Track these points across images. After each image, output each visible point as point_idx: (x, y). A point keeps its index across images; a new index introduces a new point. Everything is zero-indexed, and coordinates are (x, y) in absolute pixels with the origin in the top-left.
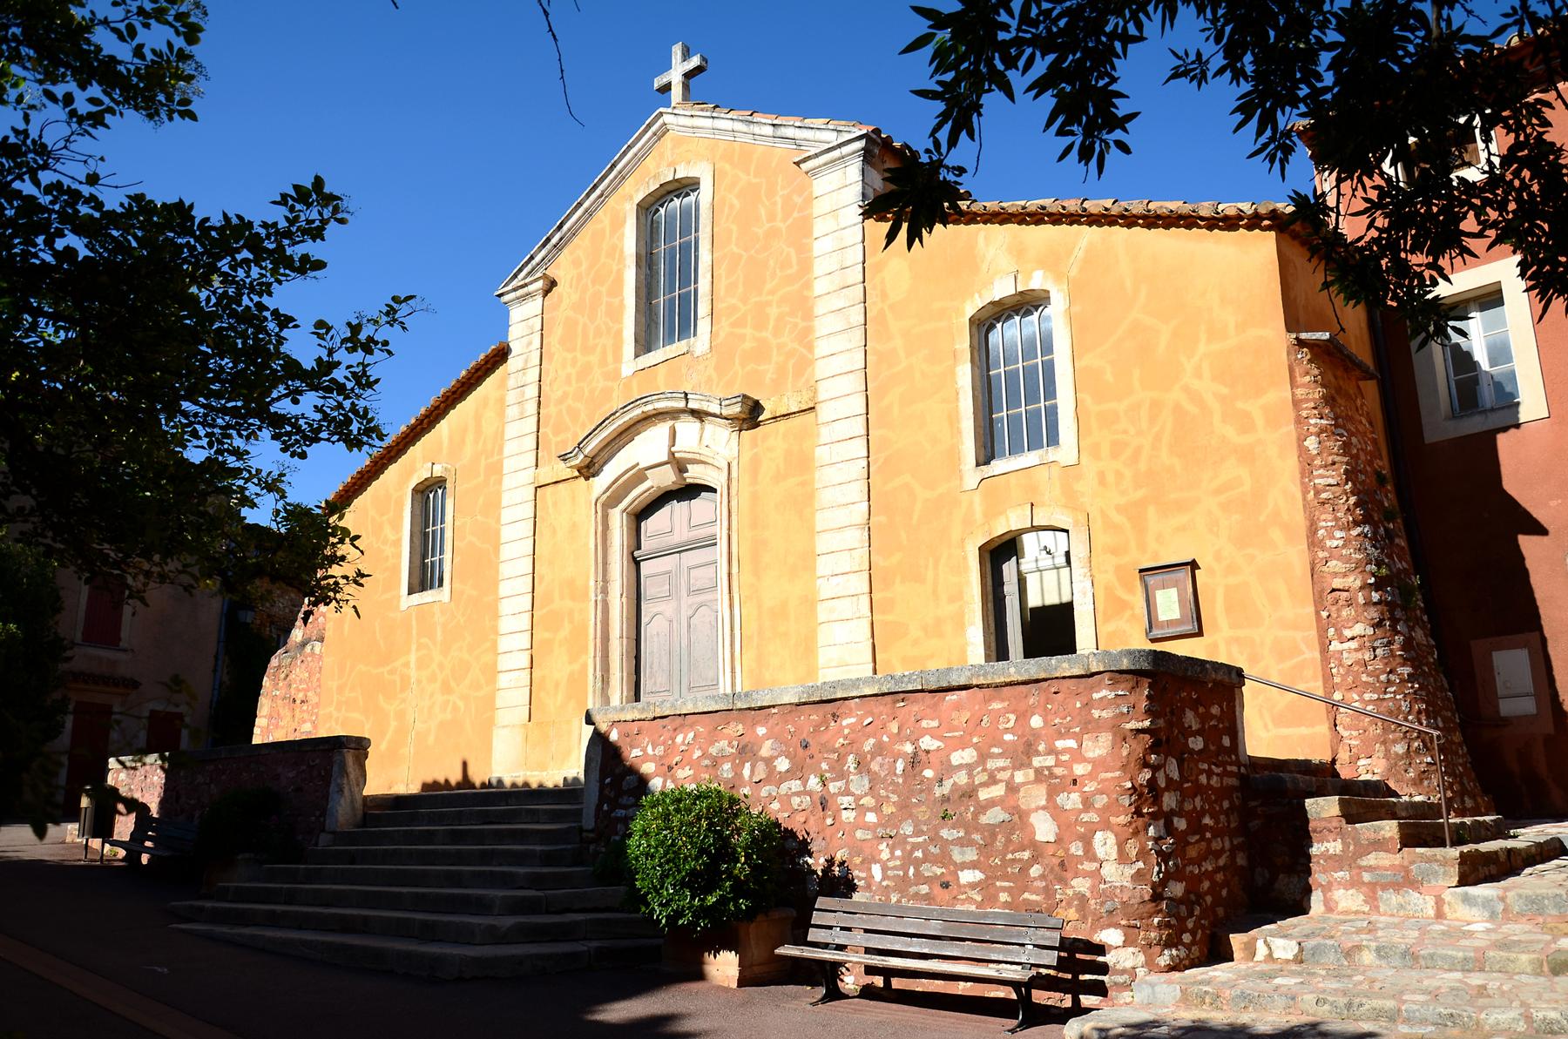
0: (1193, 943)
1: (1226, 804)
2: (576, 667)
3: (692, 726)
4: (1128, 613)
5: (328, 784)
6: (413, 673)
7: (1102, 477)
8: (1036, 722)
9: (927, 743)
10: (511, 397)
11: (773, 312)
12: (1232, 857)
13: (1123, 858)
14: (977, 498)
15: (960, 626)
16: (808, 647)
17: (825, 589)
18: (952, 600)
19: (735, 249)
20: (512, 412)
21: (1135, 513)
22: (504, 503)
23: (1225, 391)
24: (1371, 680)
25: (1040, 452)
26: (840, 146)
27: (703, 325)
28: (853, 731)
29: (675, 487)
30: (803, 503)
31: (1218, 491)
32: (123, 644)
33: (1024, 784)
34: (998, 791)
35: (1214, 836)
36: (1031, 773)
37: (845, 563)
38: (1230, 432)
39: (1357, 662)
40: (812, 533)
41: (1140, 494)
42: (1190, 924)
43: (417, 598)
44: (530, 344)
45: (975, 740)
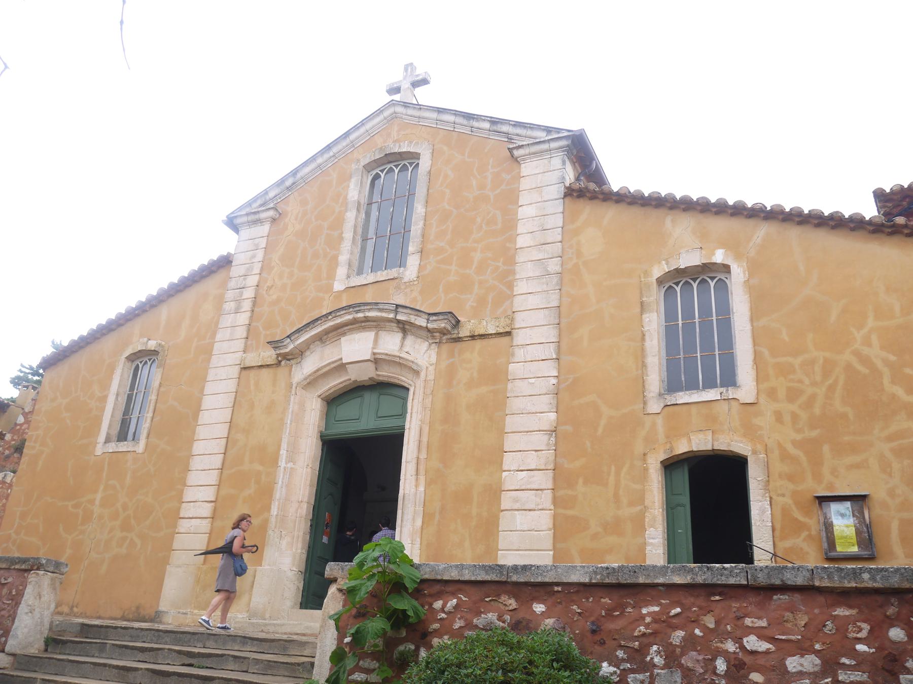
3: (454, 594)
4: (805, 534)
5: (18, 604)
6: (97, 510)
8: (896, 634)
9: (752, 642)
10: (230, 295)
11: (477, 256)
14: (659, 421)
15: (640, 526)
16: (489, 528)
17: (510, 480)
18: (631, 504)
19: (447, 207)
20: (229, 306)
22: (210, 378)
23: (893, 358)
26: (549, 141)
28: (655, 621)
30: (494, 409)
31: (890, 439)
37: (532, 461)
40: (502, 433)
41: (814, 433)
43: (112, 447)
44: (254, 256)
45: (817, 647)
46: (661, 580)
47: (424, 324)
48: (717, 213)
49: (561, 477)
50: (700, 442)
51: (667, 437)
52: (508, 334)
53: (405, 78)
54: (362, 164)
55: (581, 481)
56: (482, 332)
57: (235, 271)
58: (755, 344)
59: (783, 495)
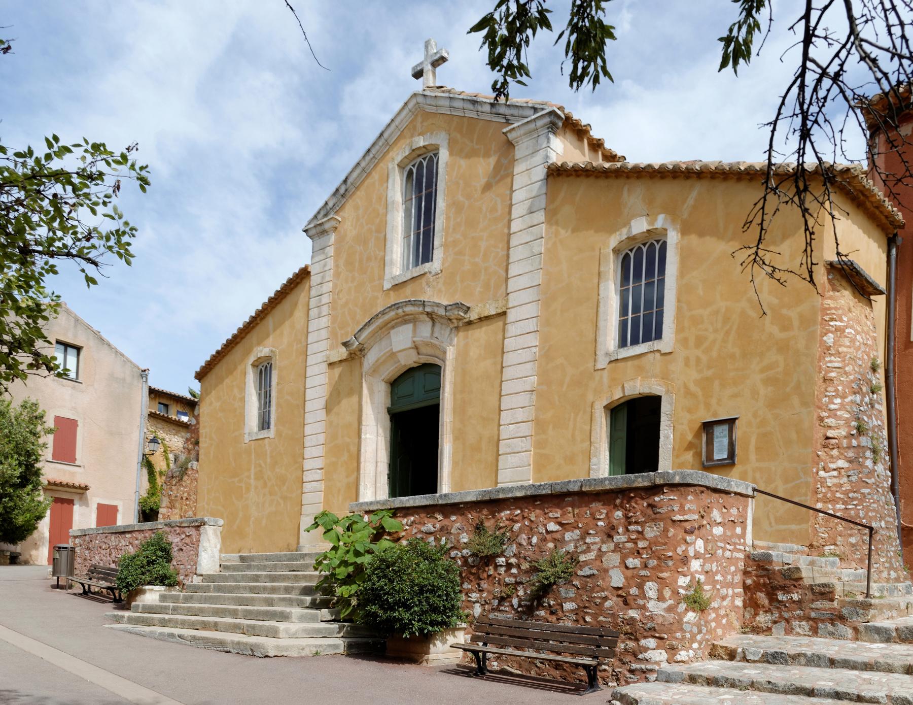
0: (699, 648)
1: (733, 568)
7: (687, 361)
12: (733, 601)
13: (661, 598)
20: (313, 313)
23: (775, 301)
24: (842, 496)
25: (650, 343)
29: (415, 365)
31: (762, 371)
32: (77, 463)
33: (606, 552)
34: (592, 556)
35: (722, 587)
36: (612, 545)
37: (520, 415)
38: (775, 330)
42: (699, 637)
46: (510, 495)
47: (443, 314)
48: (675, 177)
49: (540, 425)
50: (637, 387)
51: (610, 387)
52: (504, 313)
53: (426, 59)
54: (396, 162)
55: (551, 427)
56: (486, 314)
57: (314, 279)
58: (679, 301)
59: (682, 424)
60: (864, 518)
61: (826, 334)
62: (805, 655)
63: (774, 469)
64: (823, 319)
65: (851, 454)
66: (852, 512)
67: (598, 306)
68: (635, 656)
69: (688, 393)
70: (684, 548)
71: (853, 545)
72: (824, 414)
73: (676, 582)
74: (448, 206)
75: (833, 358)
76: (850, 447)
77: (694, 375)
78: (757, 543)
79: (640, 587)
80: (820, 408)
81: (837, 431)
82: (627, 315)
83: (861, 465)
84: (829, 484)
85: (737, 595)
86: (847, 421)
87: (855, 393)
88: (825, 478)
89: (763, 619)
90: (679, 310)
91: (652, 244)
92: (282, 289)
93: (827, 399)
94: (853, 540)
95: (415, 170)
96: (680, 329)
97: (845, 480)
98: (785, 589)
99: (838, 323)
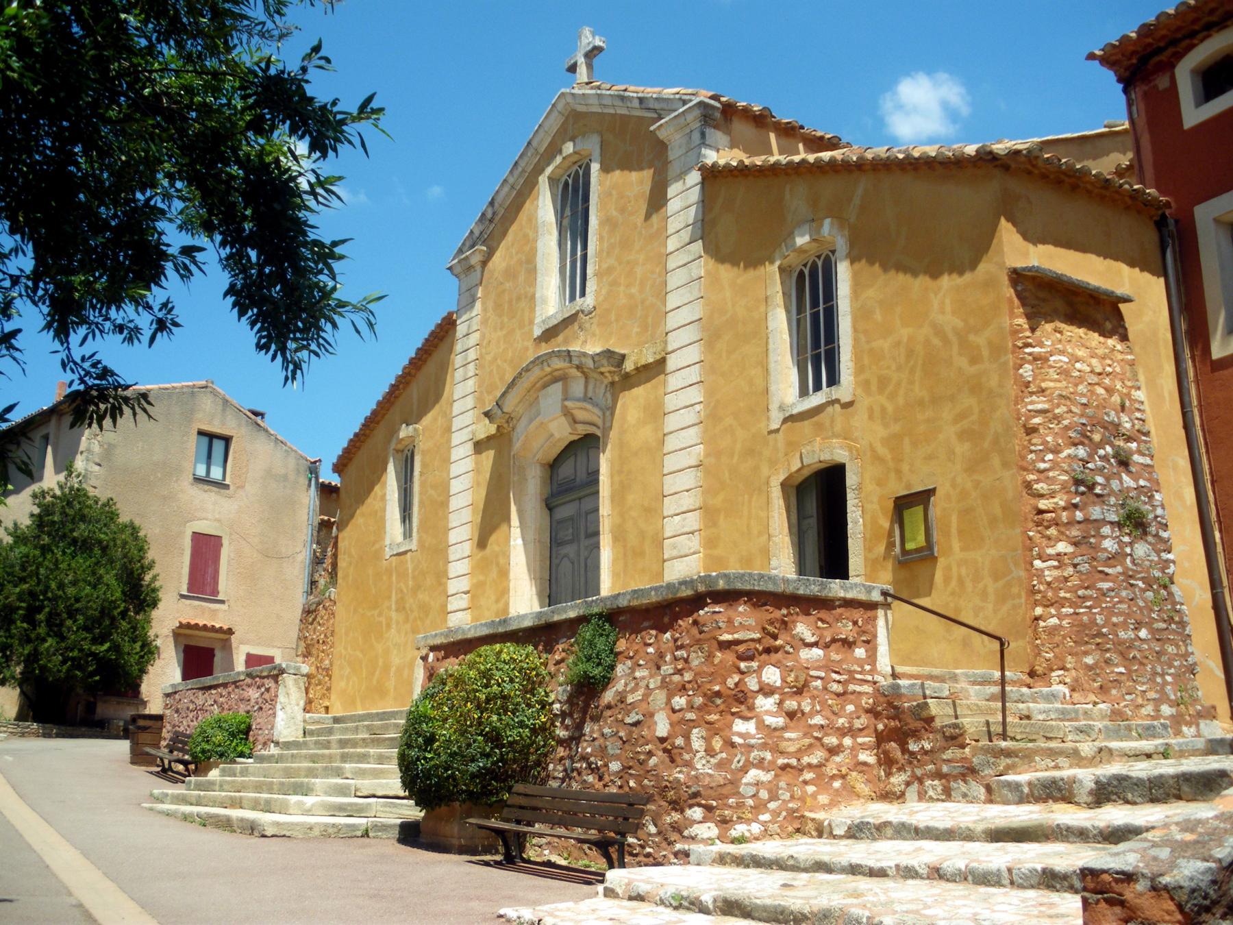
0: (773, 822)
2: (501, 605)
7: (871, 410)
13: (710, 752)
16: (661, 574)
21: (893, 442)
22: (453, 458)
23: (960, 324)
27: (591, 286)
34: (638, 696)
38: (962, 362)
39: (1056, 579)
49: (709, 513)
59: (872, 502)
60: (1104, 626)
61: (1021, 366)
62: (890, 823)
63: (980, 559)
64: (1015, 346)
65: (1075, 532)
66: (1085, 618)
67: (767, 343)
68: (680, 832)
69: (877, 458)
70: (736, 678)
71: (1090, 668)
72: (1031, 477)
73: (730, 727)
74: (601, 224)
75: (1034, 398)
76: (1072, 523)
77: (881, 432)
78: (899, 669)
79: (687, 738)
80: (1025, 469)
81: (1052, 500)
82: (826, 351)
83: (1096, 548)
84: (1049, 579)
85: (863, 747)
86: (1064, 486)
87: (1075, 445)
88: (1042, 570)
89: (898, 779)
90: (856, 340)
91: (827, 256)
92: (424, 345)
93: (1032, 456)
94: (1089, 660)
95: (570, 181)
96: (859, 370)
97: (1070, 570)
98: (915, 734)
99: (1037, 350)
